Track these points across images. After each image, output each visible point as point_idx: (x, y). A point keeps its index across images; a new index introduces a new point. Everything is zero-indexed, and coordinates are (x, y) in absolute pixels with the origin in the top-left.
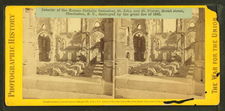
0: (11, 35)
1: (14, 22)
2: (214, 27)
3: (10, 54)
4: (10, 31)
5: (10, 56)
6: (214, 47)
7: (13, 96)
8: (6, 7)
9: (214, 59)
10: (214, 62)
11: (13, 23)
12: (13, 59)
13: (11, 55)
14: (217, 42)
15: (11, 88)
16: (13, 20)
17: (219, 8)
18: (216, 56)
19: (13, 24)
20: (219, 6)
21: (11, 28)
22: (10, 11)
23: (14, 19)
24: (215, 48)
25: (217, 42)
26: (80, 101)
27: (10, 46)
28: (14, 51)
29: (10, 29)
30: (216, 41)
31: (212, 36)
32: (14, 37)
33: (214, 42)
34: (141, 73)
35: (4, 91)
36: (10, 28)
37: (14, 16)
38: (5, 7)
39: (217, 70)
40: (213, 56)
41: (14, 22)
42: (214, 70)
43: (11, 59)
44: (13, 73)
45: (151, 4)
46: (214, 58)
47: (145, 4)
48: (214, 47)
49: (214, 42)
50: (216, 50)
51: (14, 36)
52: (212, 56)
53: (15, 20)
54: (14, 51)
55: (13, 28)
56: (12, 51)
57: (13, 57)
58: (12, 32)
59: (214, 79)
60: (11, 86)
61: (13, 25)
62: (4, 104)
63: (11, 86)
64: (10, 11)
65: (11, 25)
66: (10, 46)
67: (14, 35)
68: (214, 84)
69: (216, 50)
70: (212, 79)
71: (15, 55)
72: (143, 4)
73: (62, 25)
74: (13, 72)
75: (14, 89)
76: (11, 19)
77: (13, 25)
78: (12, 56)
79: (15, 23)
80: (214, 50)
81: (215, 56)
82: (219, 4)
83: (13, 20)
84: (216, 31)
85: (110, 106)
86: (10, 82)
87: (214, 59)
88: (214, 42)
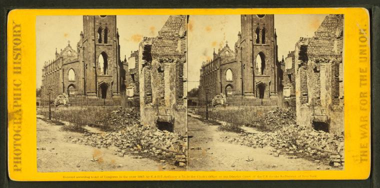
1: (20, 35)
2: (361, 46)
3: (14, 95)
4: (14, 52)
5: (14, 99)
7: (20, 170)
9: (362, 102)
10: (363, 106)
11: (18, 37)
12: (19, 168)
13: (16, 97)
15: (16, 156)
16: (18, 33)
17: (375, 12)
20: (374, 8)
21: (16, 143)
22: (16, 17)
23: (19, 31)
26: (68, 43)
27: (14, 81)
28: (20, 89)
29: (14, 49)
32: (19, 63)
36: (14, 47)
37: (19, 26)
40: (361, 97)
41: (20, 35)
42: (361, 121)
43: (16, 104)
44: (20, 129)
45: (258, 6)
47: (248, 6)
51: (19, 61)
52: (359, 96)
53: (22, 34)
54: (20, 89)
55: (18, 142)
56: (17, 158)
57: (19, 165)
59: (363, 138)
60: (16, 152)
61: (18, 42)
62: (6, 177)
63: (16, 152)
64: (16, 17)
65: (16, 42)
66: (14, 81)
67: (20, 59)
68: (362, 146)
70: (361, 138)
71: (23, 97)
72: (244, 6)
73: (189, 150)
74: (19, 127)
75: (20, 158)
76: (15, 31)
77: (18, 42)
78: (17, 162)
79: (22, 39)
80: (361, 84)
81: (364, 96)
82: (375, 5)
83: (18, 33)
86: (15, 145)
87: (362, 102)
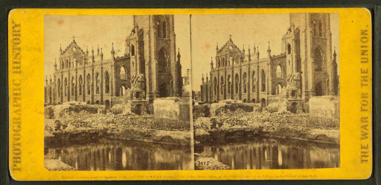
0: (18, 54)
6: (362, 156)
8: (11, 11)
11: (18, 37)
14: (367, 148)
18: (367, 34)
19: (18, 39)
22: (17, 16)
23: (19, 31)
24: (364, 159)
25: (367, 148)
30: (366, 146)
31: (362, 62)
33: (363, 71)
34: (273, 62)
35: (7, 155)
38: (10, 10)
39: (367, 122)
46: (363, 38)
48: (362, 156)
49: (362, 72)
50: (367, 161)
53: (22, 33)
58: (15, 54)
64: (17, 16)
69: (367, 161)
80: (362, 161)
84: (367, 33)
85: (178, 181)
88: (362, 72)
